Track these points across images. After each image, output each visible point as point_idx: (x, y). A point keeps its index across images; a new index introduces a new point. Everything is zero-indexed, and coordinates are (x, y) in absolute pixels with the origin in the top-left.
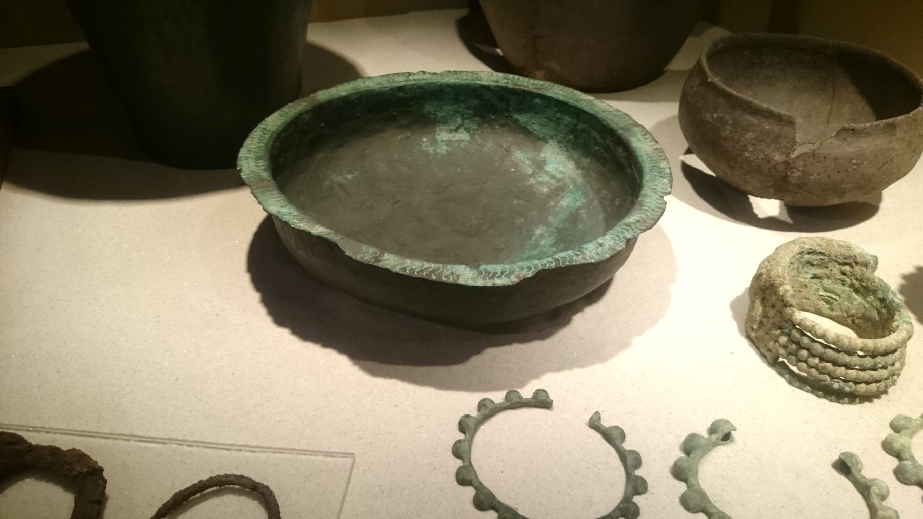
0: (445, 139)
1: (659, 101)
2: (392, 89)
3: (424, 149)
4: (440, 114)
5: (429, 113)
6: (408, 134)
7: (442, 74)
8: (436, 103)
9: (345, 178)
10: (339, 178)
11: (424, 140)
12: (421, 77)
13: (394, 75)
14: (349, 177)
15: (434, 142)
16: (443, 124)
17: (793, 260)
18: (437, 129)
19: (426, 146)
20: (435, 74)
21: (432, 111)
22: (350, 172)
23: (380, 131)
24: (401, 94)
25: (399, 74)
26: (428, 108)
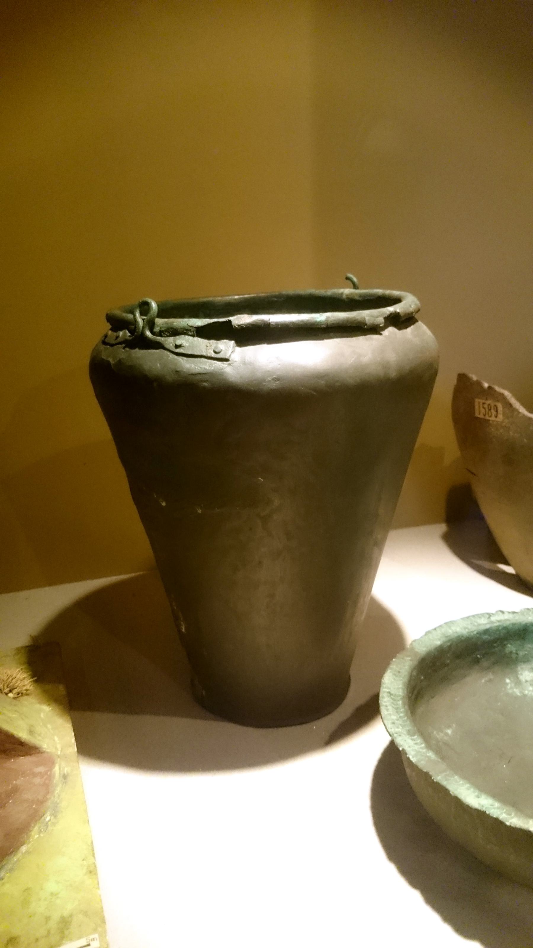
0: (528, 678)
1: (379, 561)
2: (479, 633)
3: (510, 691)
4: (521, 653)
5: (511, 652)
6: (491, 676)
7: (522, 613)
8: (518, 643)
9: (446, 734)
10: (441, 734)
11: (508, 681)
12: (501, 617)
13: (473, 616)
14: (449, 731)
15: (518, 683)
16: (524, 662)
17: (493, 634)
18: (519, 668)
19: (511, 688)
20: (514, 613)
21: (514, 650)
22: (449, 727)
23: (465, 676)
24: (485, 637)
25: (482, 615)
26: (510, 647)
